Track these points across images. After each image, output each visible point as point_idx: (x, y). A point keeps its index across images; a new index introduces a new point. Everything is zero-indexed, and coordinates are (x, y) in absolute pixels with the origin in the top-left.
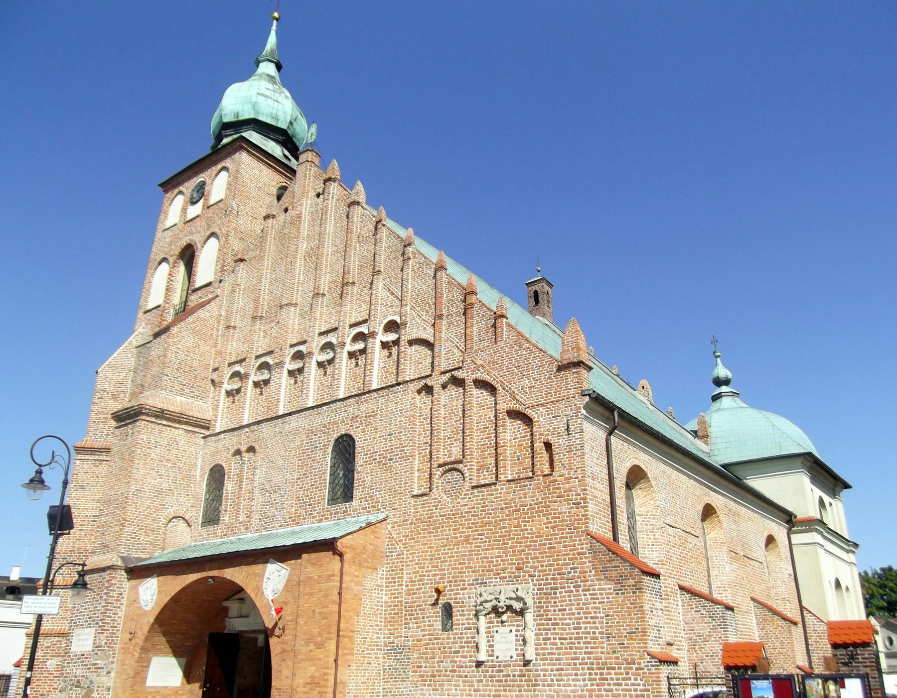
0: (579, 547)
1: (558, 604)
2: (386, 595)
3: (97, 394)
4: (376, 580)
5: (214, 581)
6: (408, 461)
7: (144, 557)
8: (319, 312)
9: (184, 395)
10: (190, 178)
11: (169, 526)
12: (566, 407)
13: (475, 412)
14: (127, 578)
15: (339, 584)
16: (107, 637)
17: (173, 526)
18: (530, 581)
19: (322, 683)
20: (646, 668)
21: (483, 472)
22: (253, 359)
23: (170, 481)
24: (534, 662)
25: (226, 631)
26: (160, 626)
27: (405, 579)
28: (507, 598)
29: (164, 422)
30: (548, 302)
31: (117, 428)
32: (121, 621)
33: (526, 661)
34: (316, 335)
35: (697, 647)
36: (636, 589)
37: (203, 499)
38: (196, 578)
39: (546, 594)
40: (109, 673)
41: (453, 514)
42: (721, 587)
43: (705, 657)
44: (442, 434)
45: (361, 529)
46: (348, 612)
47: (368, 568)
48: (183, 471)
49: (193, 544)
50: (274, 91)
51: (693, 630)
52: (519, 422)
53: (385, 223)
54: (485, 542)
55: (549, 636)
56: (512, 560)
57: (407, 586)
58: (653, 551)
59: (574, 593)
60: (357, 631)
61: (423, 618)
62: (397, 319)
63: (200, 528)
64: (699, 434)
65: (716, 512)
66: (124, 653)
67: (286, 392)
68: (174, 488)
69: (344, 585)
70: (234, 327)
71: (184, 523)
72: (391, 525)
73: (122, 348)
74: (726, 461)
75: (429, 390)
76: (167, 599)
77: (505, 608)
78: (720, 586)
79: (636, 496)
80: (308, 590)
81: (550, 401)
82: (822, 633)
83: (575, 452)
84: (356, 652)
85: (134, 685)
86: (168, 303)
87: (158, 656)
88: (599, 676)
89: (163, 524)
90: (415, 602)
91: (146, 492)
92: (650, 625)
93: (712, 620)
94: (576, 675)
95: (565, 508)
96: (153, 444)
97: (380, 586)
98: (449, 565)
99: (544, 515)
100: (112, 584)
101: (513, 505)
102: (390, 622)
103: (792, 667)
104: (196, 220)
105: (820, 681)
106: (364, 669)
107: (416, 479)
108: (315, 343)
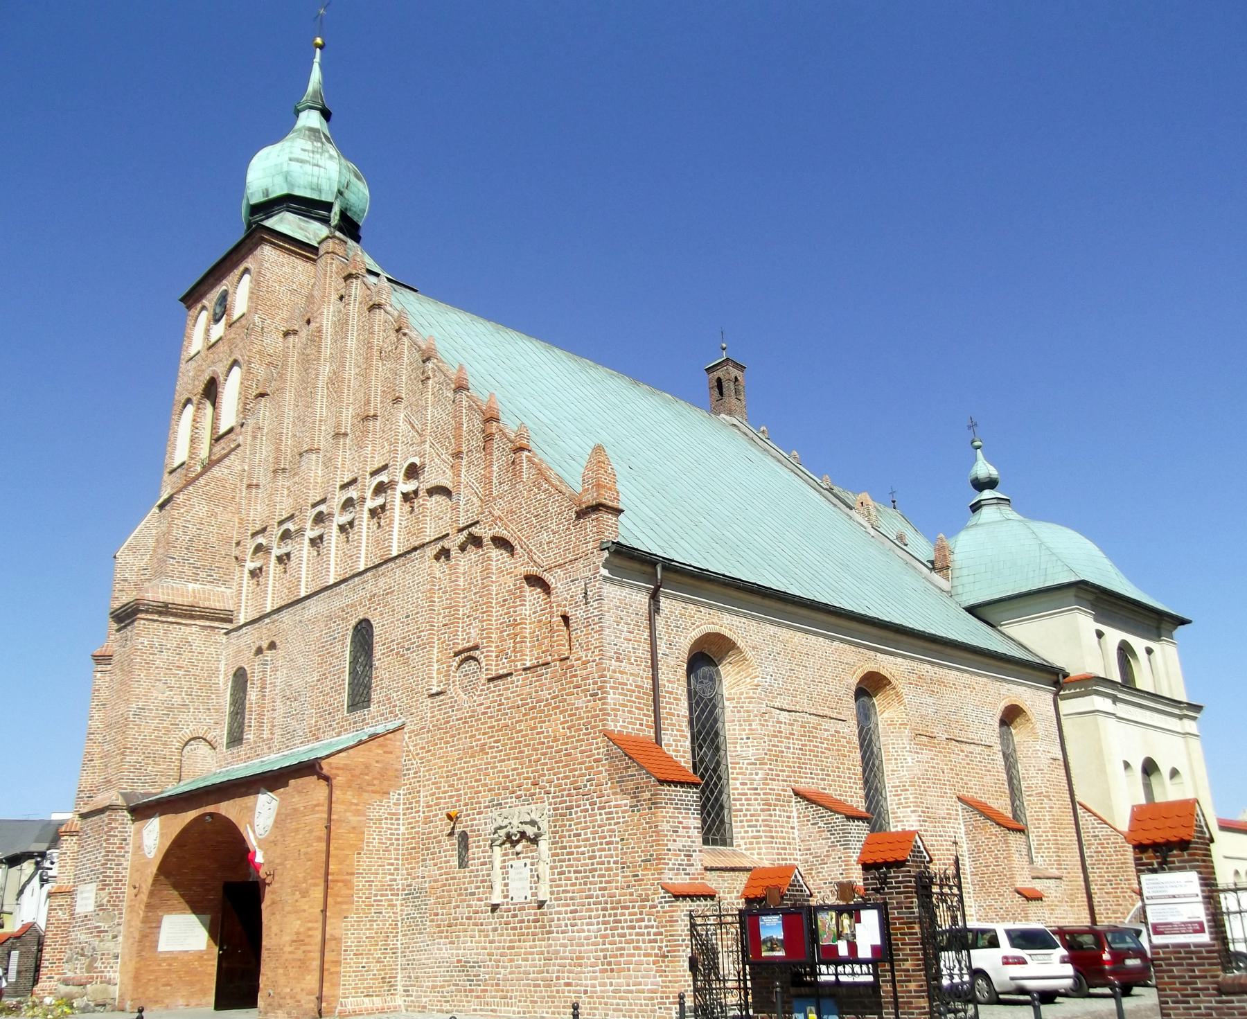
0: (596, 752)
1: (573, 827)
2: (403, 825)
3: (117, 585)
4: (388, 806)
5: (212, 818)
6: (425, 650)
7: (154, 791)
8: (340, 458)
9: (198, 580)
10: (213, 286)
11: (185, 751)
12: (584, 567)
13: (494, 579)
14: (132, 820)
15: (325, 816)
16: (110, 893)
17: (191, 750)
18: (546, 799)
19: (307, 940)
20: (659, 906)
21: (501, 659)
22: (276, 527)
23: (183, 693)
24: (548, 903)
25: (251, 880)
26: (167, 877)
27: (422, 804)
28: (521, 823)
29: (171, 619)
30: (737, 392)
31: (118, 630)
32: (127, 873)
33: (541, 901)
34: (338, 489)
35: (813, 872)
36: (652, 804)
37: (227, 713)
38: (193, 817)
39: (562, 814)
40: (115, 937)
41: (470, 717)
42: (899, 786)
43: (823, 885)
44: (461, 613)
45: (360, 743)
46: (343, 850)
47: (374, 792)
48: (201, 679)
49: (218, 771)
50: (313, 152)
51: (810, 849)
52: (539, 590)
53: (406, 331)
54: (501, 751)
55: (564, 869)
56: (528, 773)
57: (424, 812)
58: (749, 747)
59: (590, 812)
60: (357, 873)
61: (440, 853)
62: (417, 461)
63: (225, 750)
64: (938, 565)
65: (890, 683)
66: (131, 912)
67: (337, 564)
68: (190, 702)
69: (334, 817)
70: (257, 486)
71: (205, 745)
72: (408, 735)
73: (143, 523)
74: (972, 602)
75: (444, 553)
76: (168, 844)
77: (518, 835)
78: (898, 784)
79: (725, 674)
80: (294, 825)
81: (567, 560)
82: (1104, 839)
83: (593, 626)
84: (356, 899)
85: (142, 950)
86: (193, 458)
87: (171, 914)
88: (612, 918)
89: (177, 749)
90: (431, 833)
91: (152, 710)
92: (669, 850)
93: (831, 834)
94: (590, 917)
95: (580, 703)
96: (157, 648)
97: (394, 814)
98: (466, 783)
99: (561, 712)
100: (112, 828)
101: (529, 701)
102: (407, 859)
103: (1010, 892)
104: (218, 345)
105: (834, 914)
106: (370, 921)
107: (435, 673)
108: (336, 500)
